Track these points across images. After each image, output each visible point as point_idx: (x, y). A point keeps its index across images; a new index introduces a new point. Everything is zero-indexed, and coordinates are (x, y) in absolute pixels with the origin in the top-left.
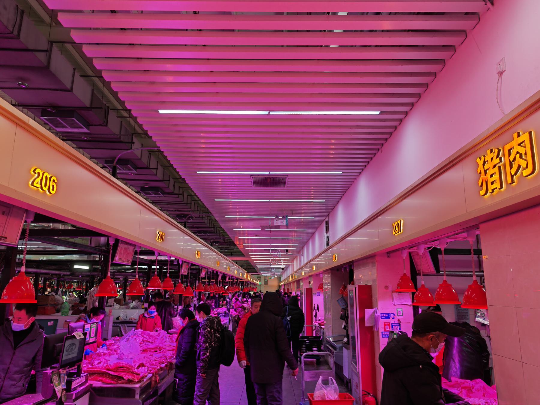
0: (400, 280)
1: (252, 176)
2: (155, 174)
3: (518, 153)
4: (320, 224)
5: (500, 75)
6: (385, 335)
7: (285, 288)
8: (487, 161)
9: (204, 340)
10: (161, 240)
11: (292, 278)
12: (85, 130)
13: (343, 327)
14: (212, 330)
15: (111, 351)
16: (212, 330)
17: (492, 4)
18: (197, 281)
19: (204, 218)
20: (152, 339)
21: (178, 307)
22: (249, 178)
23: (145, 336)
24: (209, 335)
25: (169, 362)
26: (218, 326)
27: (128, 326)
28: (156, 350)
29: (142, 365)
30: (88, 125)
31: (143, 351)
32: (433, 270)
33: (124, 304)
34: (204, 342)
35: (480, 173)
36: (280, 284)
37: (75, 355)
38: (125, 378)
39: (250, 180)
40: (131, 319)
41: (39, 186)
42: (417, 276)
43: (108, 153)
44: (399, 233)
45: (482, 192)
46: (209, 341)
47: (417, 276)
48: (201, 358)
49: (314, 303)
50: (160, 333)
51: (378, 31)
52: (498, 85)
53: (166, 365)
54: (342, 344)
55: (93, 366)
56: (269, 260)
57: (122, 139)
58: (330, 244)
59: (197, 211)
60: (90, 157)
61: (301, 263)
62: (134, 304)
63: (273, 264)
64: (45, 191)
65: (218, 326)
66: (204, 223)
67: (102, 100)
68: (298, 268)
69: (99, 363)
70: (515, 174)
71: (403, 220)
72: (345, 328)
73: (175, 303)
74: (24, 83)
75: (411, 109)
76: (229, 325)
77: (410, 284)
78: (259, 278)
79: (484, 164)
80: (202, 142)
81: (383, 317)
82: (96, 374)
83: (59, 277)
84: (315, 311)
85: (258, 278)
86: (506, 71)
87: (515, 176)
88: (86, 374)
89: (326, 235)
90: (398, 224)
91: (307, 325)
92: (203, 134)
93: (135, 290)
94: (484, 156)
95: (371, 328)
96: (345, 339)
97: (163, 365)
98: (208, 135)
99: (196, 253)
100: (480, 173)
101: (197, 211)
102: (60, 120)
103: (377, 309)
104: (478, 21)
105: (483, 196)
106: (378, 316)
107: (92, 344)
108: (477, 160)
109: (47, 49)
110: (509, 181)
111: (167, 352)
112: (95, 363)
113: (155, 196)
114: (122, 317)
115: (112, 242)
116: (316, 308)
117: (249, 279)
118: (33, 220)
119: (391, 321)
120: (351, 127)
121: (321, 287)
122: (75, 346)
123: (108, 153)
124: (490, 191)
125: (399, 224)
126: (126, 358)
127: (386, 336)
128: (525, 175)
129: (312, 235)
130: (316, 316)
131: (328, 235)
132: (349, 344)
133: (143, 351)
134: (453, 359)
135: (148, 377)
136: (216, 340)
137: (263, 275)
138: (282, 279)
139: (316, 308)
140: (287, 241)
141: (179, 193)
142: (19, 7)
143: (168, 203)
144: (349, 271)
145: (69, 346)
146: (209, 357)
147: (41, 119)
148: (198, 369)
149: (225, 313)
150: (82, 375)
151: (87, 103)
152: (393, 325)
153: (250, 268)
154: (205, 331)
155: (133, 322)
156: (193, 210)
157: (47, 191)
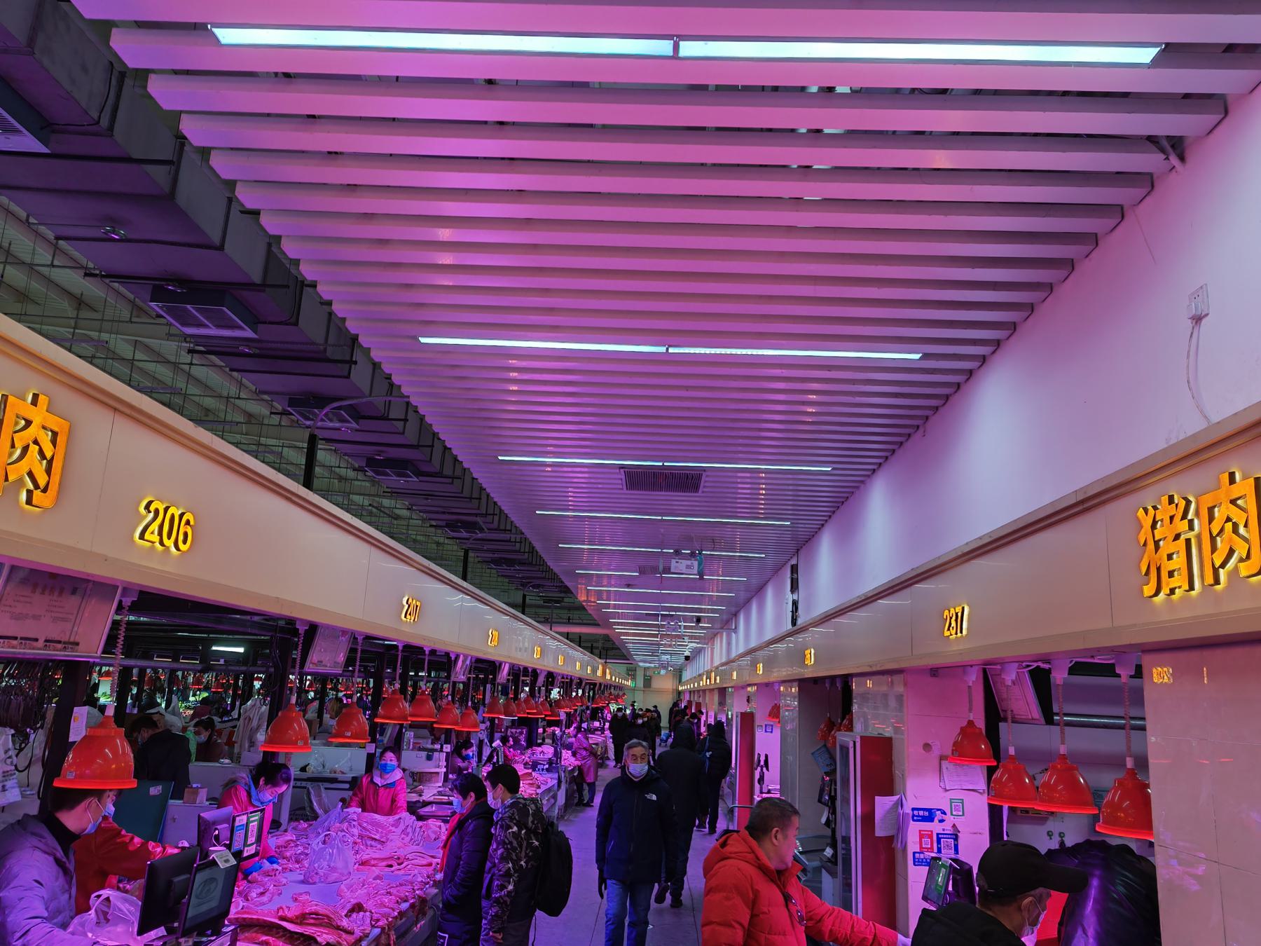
0: (959, 734)
1: (622, 468)
2: (401, 431)
3: (1228, 519)
4: (777, 569)
5: (1196, 323)
6: (920, 860)
7: (692, 699)
8: (1162, 520)
9: (502, 854)
10: (413, 618)
11: (708, 680)
12: (249, 334)
13: (824, 820)
14: (523, 832)
15: (289, 861)
16: (523, 832)
17: (1182, 158)
18: (487, 685)
19: (508, 530)
20: (382, 833)
21: (442, 747)
22: (617, 473)
23: (365, 825)
24: (515, 844)
25: (418, 896)
26: (536, 822)
27: (326, 789)
28: (390, 863)
29: (358, 908)
30: (254, 321)
31: (359, 865)
32: (1036, 712)
33: (319, 733)
34: (504, 859)
35: (1145, 544)
36: (680, 688)
37: (214, 904)
38: (318, 939)
39: (620, 476)
40: (335, 773)
41: (156, 538)
42: (1000, 724)
43: (295, 384)
44: (959, 634)
45: (1148, 590)
46: (514, 857)
47: (1000, 724)
48: (493, 896)
49: (757, 751)
50: (400, 818)
51: (926, 133)
52: (1190, 346)
53: (412, 906)
54: (821, 862)
55: (248, 900)
56: (656, 636)
57: (329, 354)
58: (799, 622)
59: (494, 514)
60: (256, 389)
61: (731, 649)
63: (665, 645)
64: (167, 548)
65: (536, 822)
66: (510, 541)
67: (288, 266)
68: (724, 660)
69: (262, 894)
70: (1223, 565)
71: (968, 605)
72: (828, 823)
73: (435, 732)
74: (117, 230)
75: (994, 352)
76: (558, 790)
77: (983, 747)
78: (631, 673)
79: (1154, 526)
80: (512, 390)
81: (916, 816)
82: (256, 926)
84: (759, 768)
85: (628, 670)
86: (1209, 316)
87: (1221, 570)
88: (232, 927)
89: (790, 597)
90: (957, 614)
91: (739, 804)
92: (514, 361)
93: (348, 731)
94: (1155, 508)
95: (890, 840)
96: (829, 852)
97: (405, 906)
98: (526, 377)
99: (489, 636)
100: (1145, 544)
101: (494, 514)
102: (191, 309)
103: (903, 796)
104: (1150, 189)
105: (1151, 597)
106: (905, 815)
107: (250, 859)
108: (1139, 512)
109: (171, 159)
110: (1210, 579)
111: (416, 871)
112: (254, 895)
113: (398, 478)
116: (762, 763)
117: (608, 677)
118: (136, 599)
119: (935, 827)
120: (854, 382)
121: (775, 713)
122: (215, 883)
123: (295, 384)
124: (1165, 590)
125: (959, 615)
126: (322, 882)
127: (922, 862)
128: (1243, 573)
129: (759, 590)
130: (761, 780)
131: (795, 597)
132: (836, 863)
133: (359, 865)
134: (1083, 926)
135: (370, 937)
136: (531, 854)
137: (641, 664)
138: (687, 675)
139: (762, 763)
140: (699, 600)
141: (454, 473)
142: (115, 65)
143: (428, 495)
144: (843, 688)
145: (202, 886)
146: (513, 894)
147: (149, 306)
148: (486, 919)
149: (550, 762)
150: (225, 930)
151: (257, 277)
152: (940, 836)
153: (607, 649)
154: (506, 832)
155: (339, 780)
156: (484, 512)
157: (172, 545)
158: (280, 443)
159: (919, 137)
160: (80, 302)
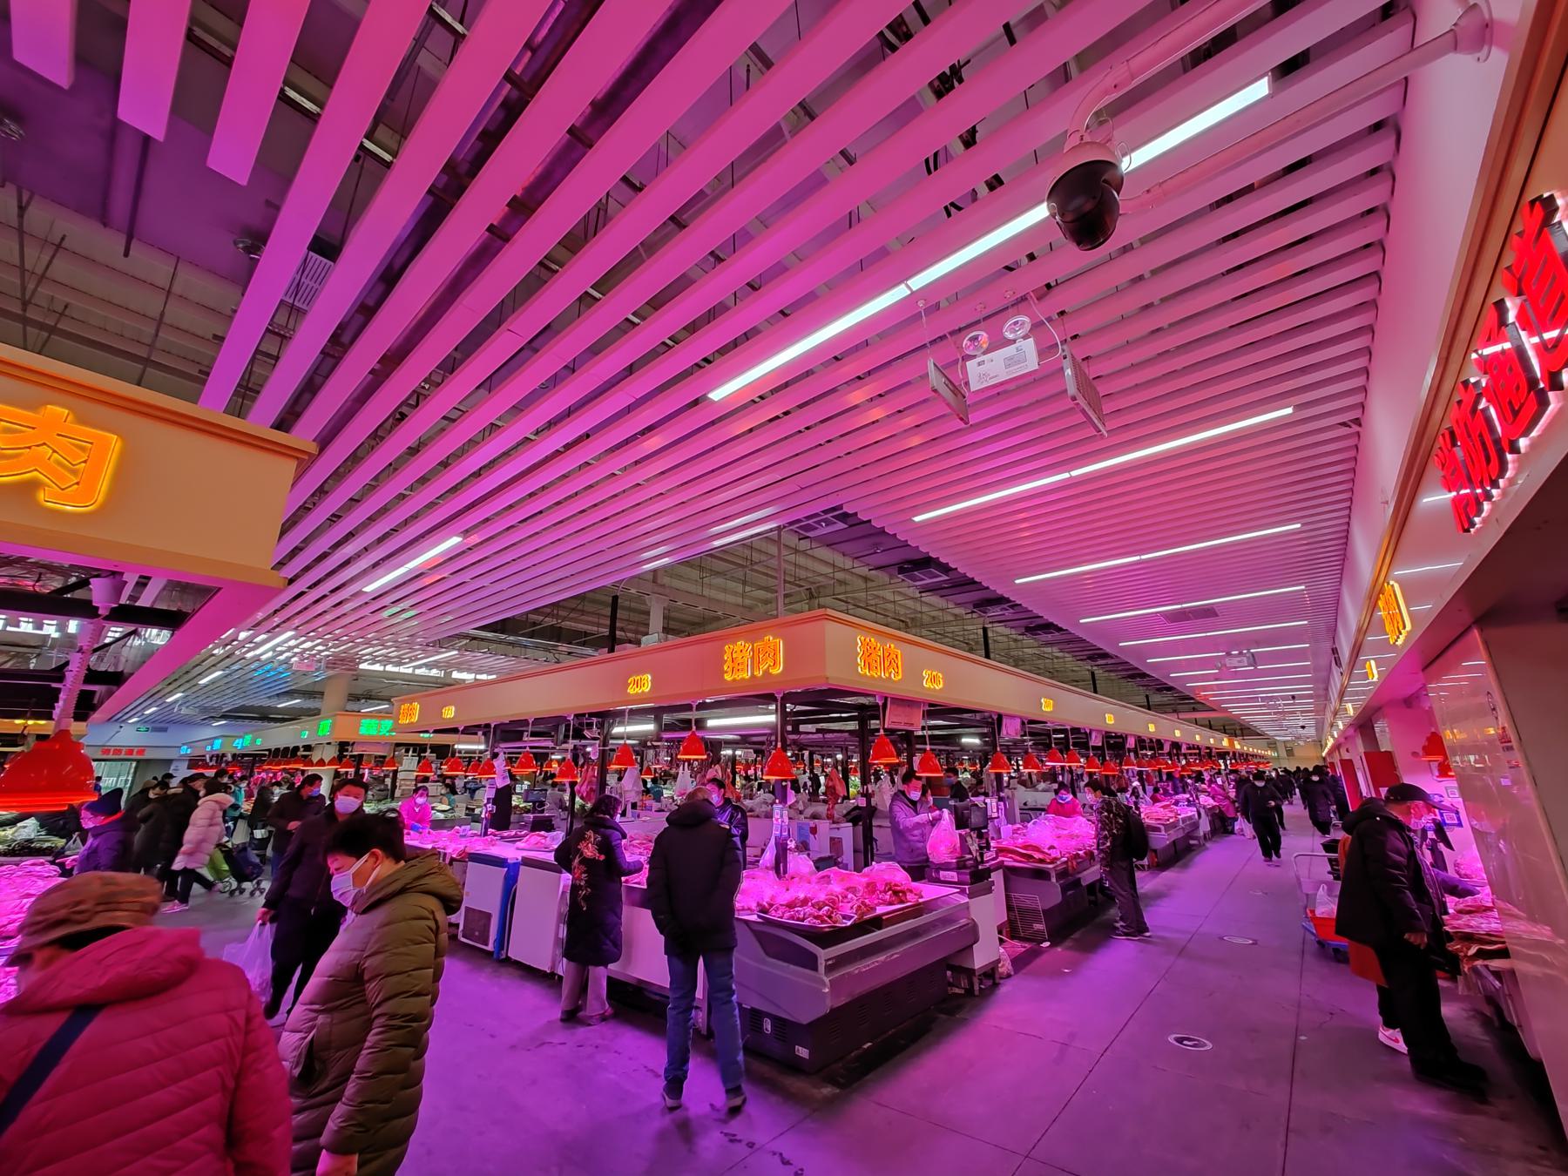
29: (1052, 847)
62: (1042, 785)
83: (948, 753)
85: (1269, 744)
114: (1031, 804)
115: (995, 717)
158: (975, 627)
159: (1057, 538)
160: (866, 579)
